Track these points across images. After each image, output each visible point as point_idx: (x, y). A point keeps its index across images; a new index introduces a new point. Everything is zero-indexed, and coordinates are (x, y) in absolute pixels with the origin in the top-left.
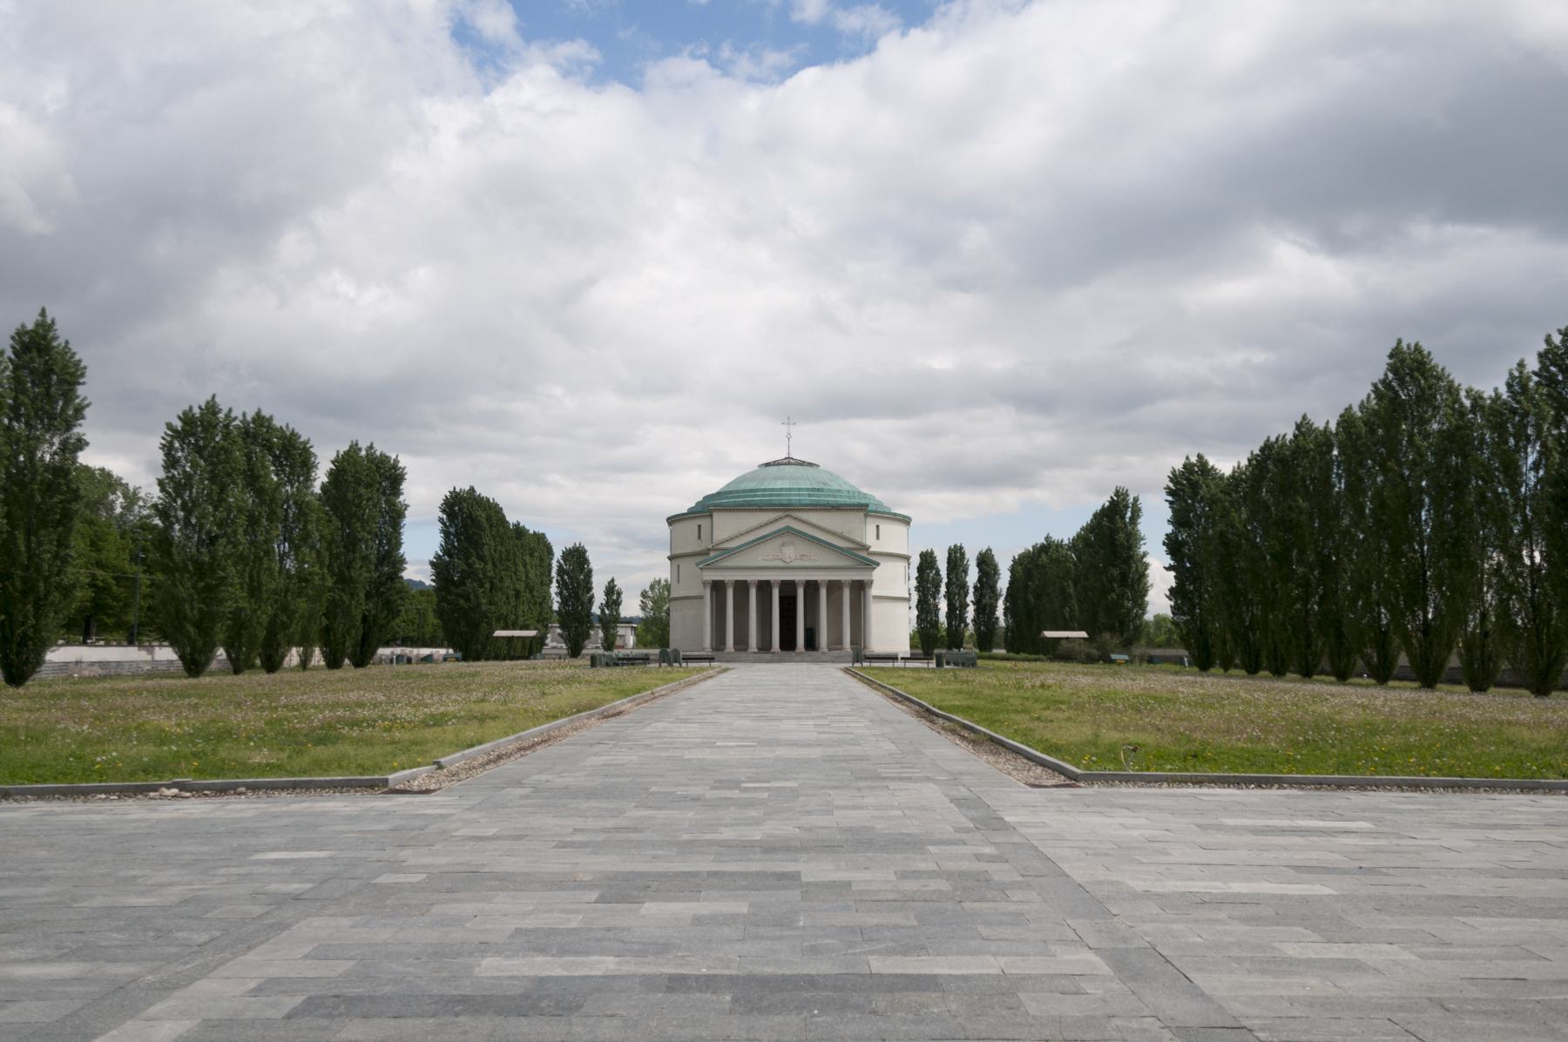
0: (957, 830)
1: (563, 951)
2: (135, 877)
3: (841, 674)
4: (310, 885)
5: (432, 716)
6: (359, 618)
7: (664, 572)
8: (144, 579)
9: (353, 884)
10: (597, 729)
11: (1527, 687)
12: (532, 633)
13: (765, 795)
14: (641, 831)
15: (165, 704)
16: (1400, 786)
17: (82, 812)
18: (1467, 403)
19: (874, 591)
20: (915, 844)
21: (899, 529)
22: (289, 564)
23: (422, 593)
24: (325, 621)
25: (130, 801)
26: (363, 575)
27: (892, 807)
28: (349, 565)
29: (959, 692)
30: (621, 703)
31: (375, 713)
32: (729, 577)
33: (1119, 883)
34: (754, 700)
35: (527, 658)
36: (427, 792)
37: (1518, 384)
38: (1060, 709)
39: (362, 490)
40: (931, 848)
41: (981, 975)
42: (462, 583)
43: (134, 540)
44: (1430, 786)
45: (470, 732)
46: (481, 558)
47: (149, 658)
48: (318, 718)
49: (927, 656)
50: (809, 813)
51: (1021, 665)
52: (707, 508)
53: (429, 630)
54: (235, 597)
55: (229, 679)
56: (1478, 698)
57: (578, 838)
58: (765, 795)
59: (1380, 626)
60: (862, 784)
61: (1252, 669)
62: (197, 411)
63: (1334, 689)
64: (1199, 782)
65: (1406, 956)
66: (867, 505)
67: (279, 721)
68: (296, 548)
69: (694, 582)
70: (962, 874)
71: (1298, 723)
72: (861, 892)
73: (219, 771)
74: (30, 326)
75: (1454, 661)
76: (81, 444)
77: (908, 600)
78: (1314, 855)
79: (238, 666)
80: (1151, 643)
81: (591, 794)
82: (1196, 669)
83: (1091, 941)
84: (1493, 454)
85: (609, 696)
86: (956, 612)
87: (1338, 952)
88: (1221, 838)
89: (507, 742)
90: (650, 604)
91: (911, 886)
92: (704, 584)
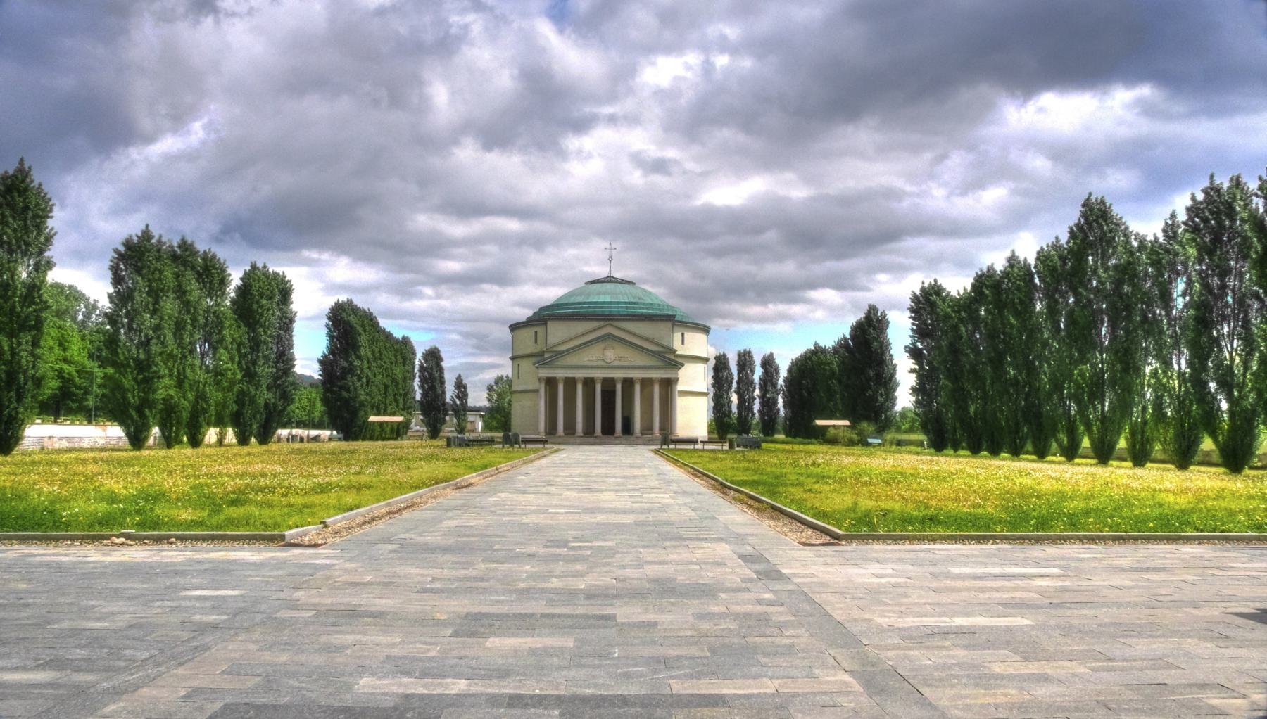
0: (744, 581)
1: (424, 674)
2: (93, 607)
3: (652, 455)
4: (225, 617)
5: (320, 485)
6: (262, 404)
7: (507, 370)
8: (99, 372)
9: (258, 618)
10: (449, 496)
11: (1173, 463)
12: (400, 419)
13: (589, 553)
14: (488, 580)
15: (115, 471)
16: (1080, 539)
17: (53, 555)
18: (1135, 244)
19: (680, 387)
20: (707, 591)
21: (701, 337)
22: (208, 361)
23: (312, 385)
24: (235, 407)
25: (89, 547)
26: (265, 371)
27: (691, 563)
28: (254, 363)
29: (747, 469)
30: (472, 477)
31: (275, 482)
32: (560, 374)
33: (870, 620)
34: (580, 475)
35: (395, 439)
36: (316, 546)
37: (1170, 230)
38: (827, 483)
39: (264, 302)
40: (723, 595)
41: (759, 695)
42: (343, 377)
43: (91, 342)
44: (1103, 539)
45: (349, 499)
46: (359, 358)
47: (103, 434)
48: (230, 485)
49: (722, 440)
50: (624, 567)
51: (796, 447)
52: (543, 317)
53: (317, 415)
54: (164, 389)
55: (162, 453)
56: (1139, 471)
57: (437, 585)
58: (589, 553)
59: (1069, 416)
60: (668, 544)
61: (975, 450)
62: (135, 239)
63: (1035, 465)
64: (933, 540)
65: (1082, 670)
66: (674, 316)
67: (200, 485)
68: (214, 348)
69: (531, 377)
70: (747, 616)
71: (1008, 492)
72: (665, 630)
73: (156, 525)
74: (11, 172)
75: (1122, 444)
76: (49, 265)
77: (705, 394)
78: (1018, 595)
79: (169, 441)
80: (898, 430)
81: (446, 550)
82: (933, 451)
83: (845, 665)
84: (1153, 284)
85: (461, 471)
86: (745, 405)
87: (1032, 668)
88: (949, 583)
89: (380, 507)
90: (495, 396)
91: (705, 626)
92: (540, 380)
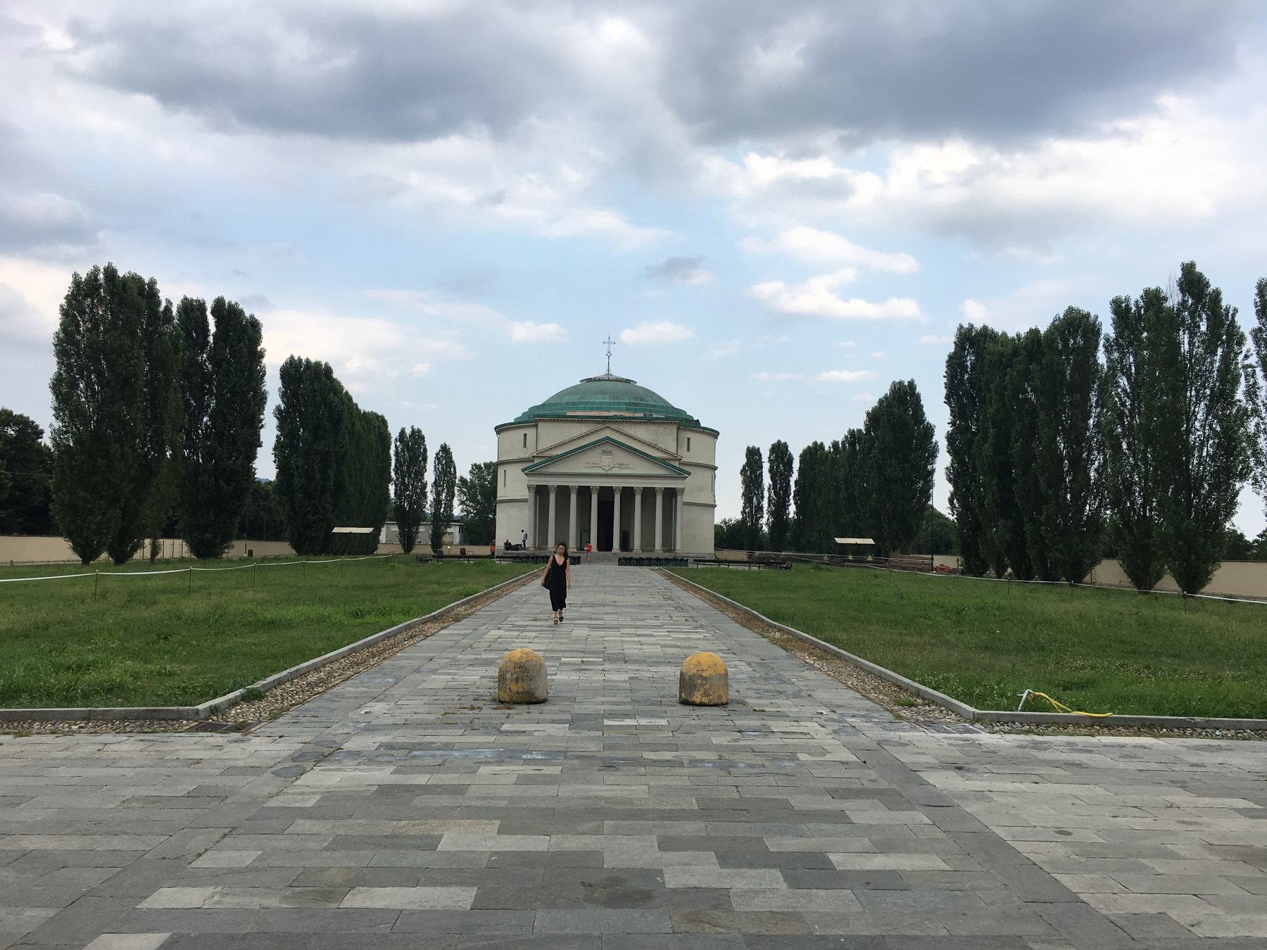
19: (686, 498)
52: (534, 419)
61: (1024, 573)
